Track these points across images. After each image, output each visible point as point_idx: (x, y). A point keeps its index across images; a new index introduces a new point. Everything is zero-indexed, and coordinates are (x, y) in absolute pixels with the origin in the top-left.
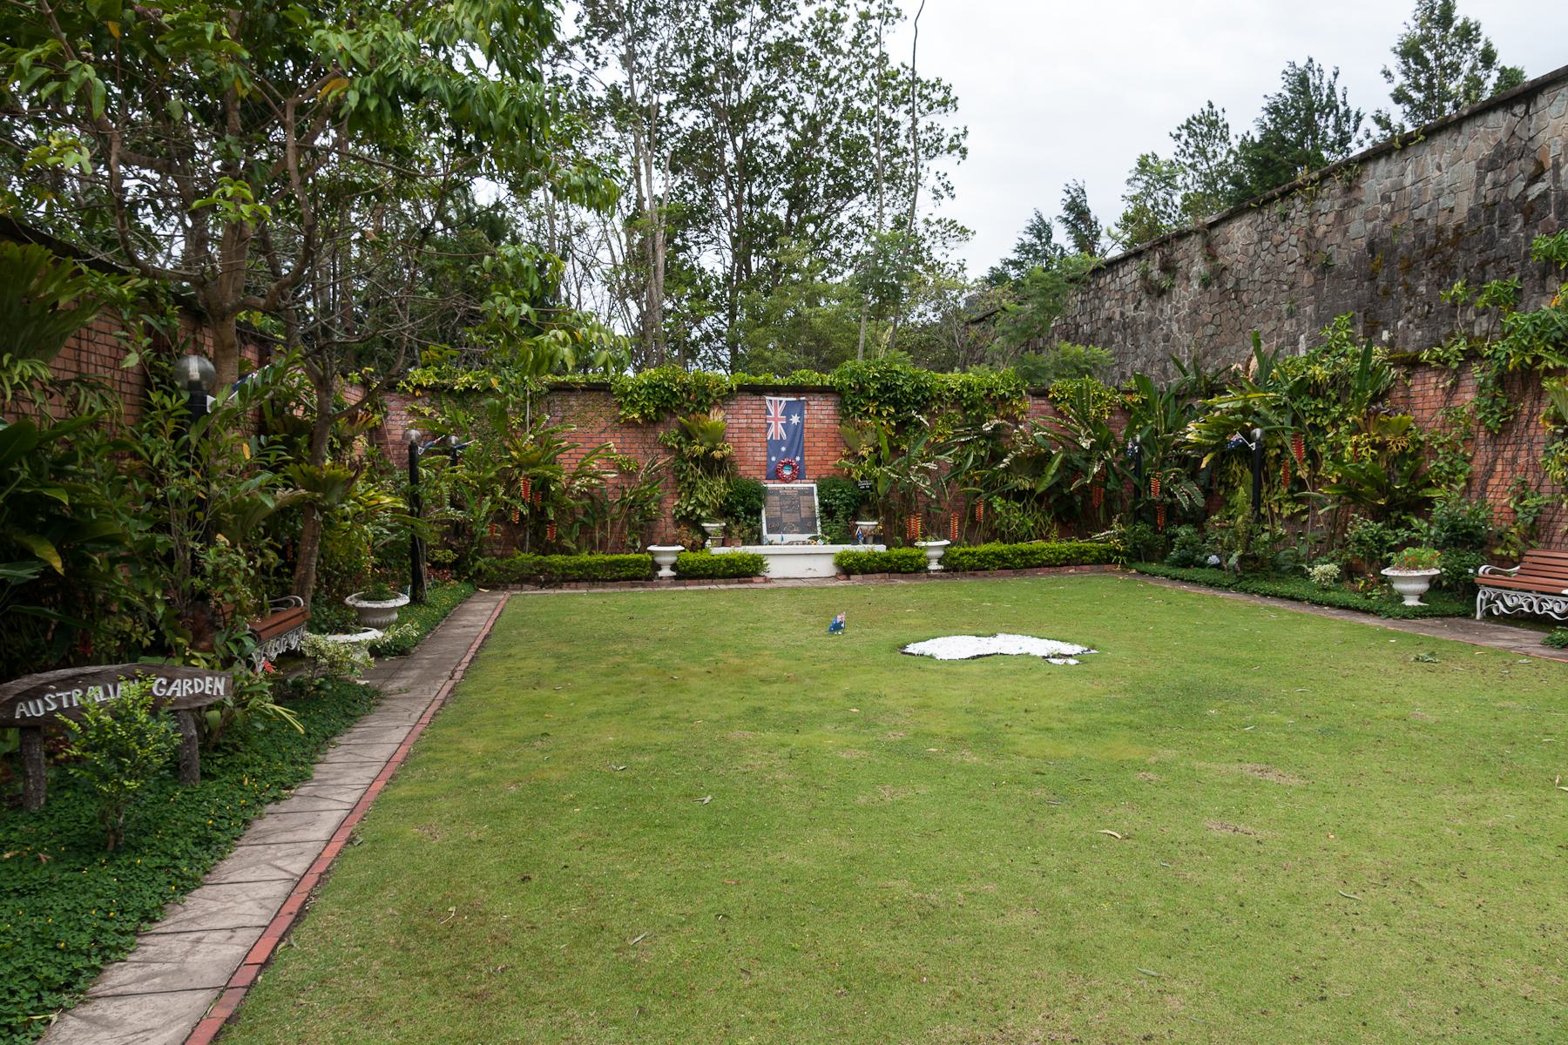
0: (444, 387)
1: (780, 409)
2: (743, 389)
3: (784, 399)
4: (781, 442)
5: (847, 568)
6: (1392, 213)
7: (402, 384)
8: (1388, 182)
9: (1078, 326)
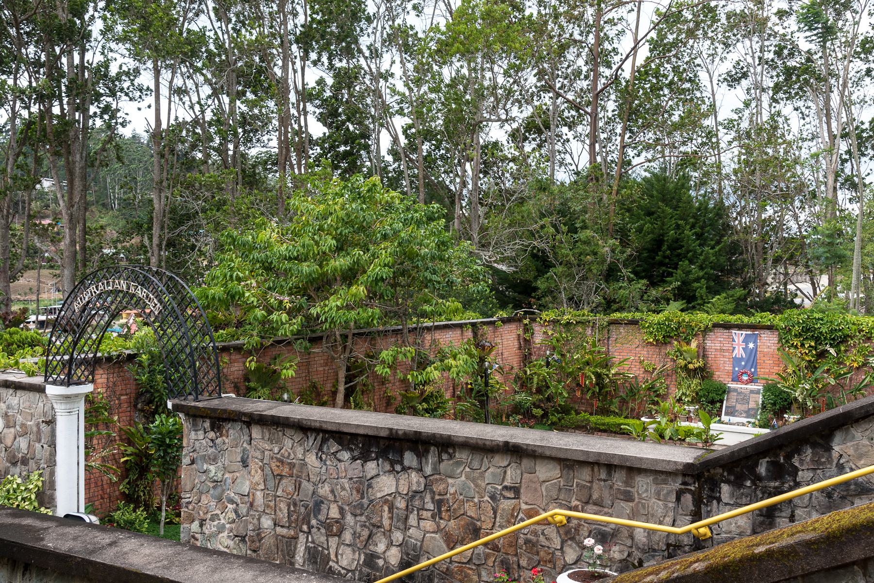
0: (558, 321)
1: (741, 339)
2: (716, 325)
3: (744, 333)
4: (742, 359)
7: (538, 319)
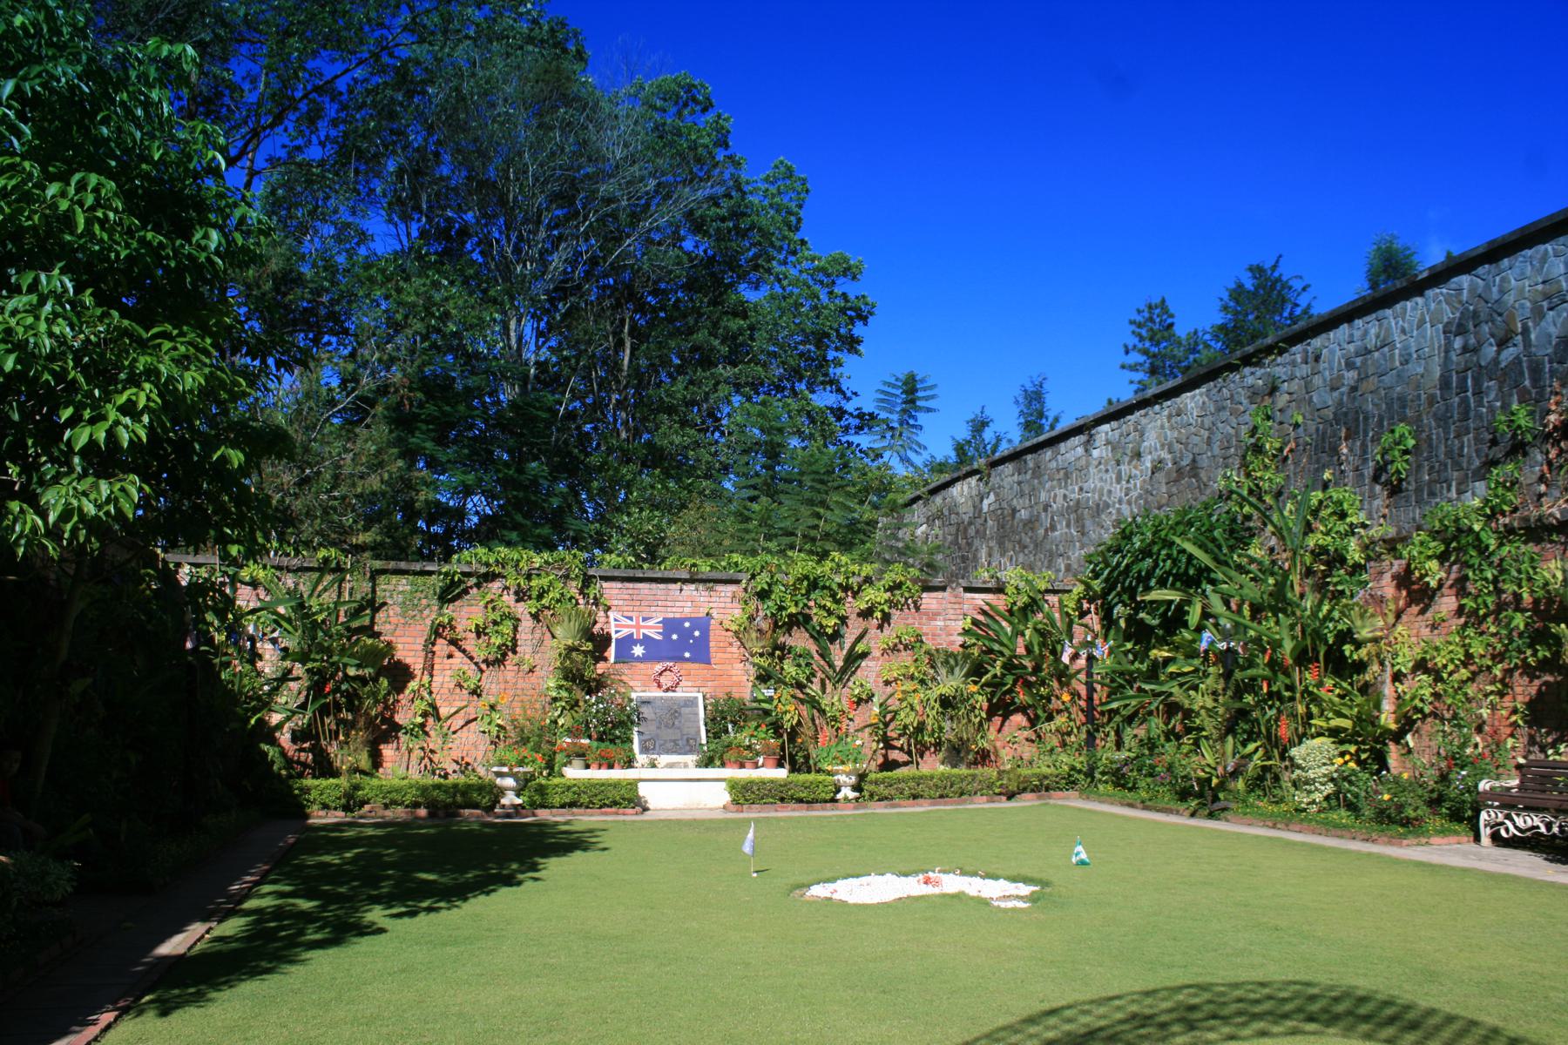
5: (744, 794)
6: (1360, 380)
8: (1351, 347)
9: (1014, 511)
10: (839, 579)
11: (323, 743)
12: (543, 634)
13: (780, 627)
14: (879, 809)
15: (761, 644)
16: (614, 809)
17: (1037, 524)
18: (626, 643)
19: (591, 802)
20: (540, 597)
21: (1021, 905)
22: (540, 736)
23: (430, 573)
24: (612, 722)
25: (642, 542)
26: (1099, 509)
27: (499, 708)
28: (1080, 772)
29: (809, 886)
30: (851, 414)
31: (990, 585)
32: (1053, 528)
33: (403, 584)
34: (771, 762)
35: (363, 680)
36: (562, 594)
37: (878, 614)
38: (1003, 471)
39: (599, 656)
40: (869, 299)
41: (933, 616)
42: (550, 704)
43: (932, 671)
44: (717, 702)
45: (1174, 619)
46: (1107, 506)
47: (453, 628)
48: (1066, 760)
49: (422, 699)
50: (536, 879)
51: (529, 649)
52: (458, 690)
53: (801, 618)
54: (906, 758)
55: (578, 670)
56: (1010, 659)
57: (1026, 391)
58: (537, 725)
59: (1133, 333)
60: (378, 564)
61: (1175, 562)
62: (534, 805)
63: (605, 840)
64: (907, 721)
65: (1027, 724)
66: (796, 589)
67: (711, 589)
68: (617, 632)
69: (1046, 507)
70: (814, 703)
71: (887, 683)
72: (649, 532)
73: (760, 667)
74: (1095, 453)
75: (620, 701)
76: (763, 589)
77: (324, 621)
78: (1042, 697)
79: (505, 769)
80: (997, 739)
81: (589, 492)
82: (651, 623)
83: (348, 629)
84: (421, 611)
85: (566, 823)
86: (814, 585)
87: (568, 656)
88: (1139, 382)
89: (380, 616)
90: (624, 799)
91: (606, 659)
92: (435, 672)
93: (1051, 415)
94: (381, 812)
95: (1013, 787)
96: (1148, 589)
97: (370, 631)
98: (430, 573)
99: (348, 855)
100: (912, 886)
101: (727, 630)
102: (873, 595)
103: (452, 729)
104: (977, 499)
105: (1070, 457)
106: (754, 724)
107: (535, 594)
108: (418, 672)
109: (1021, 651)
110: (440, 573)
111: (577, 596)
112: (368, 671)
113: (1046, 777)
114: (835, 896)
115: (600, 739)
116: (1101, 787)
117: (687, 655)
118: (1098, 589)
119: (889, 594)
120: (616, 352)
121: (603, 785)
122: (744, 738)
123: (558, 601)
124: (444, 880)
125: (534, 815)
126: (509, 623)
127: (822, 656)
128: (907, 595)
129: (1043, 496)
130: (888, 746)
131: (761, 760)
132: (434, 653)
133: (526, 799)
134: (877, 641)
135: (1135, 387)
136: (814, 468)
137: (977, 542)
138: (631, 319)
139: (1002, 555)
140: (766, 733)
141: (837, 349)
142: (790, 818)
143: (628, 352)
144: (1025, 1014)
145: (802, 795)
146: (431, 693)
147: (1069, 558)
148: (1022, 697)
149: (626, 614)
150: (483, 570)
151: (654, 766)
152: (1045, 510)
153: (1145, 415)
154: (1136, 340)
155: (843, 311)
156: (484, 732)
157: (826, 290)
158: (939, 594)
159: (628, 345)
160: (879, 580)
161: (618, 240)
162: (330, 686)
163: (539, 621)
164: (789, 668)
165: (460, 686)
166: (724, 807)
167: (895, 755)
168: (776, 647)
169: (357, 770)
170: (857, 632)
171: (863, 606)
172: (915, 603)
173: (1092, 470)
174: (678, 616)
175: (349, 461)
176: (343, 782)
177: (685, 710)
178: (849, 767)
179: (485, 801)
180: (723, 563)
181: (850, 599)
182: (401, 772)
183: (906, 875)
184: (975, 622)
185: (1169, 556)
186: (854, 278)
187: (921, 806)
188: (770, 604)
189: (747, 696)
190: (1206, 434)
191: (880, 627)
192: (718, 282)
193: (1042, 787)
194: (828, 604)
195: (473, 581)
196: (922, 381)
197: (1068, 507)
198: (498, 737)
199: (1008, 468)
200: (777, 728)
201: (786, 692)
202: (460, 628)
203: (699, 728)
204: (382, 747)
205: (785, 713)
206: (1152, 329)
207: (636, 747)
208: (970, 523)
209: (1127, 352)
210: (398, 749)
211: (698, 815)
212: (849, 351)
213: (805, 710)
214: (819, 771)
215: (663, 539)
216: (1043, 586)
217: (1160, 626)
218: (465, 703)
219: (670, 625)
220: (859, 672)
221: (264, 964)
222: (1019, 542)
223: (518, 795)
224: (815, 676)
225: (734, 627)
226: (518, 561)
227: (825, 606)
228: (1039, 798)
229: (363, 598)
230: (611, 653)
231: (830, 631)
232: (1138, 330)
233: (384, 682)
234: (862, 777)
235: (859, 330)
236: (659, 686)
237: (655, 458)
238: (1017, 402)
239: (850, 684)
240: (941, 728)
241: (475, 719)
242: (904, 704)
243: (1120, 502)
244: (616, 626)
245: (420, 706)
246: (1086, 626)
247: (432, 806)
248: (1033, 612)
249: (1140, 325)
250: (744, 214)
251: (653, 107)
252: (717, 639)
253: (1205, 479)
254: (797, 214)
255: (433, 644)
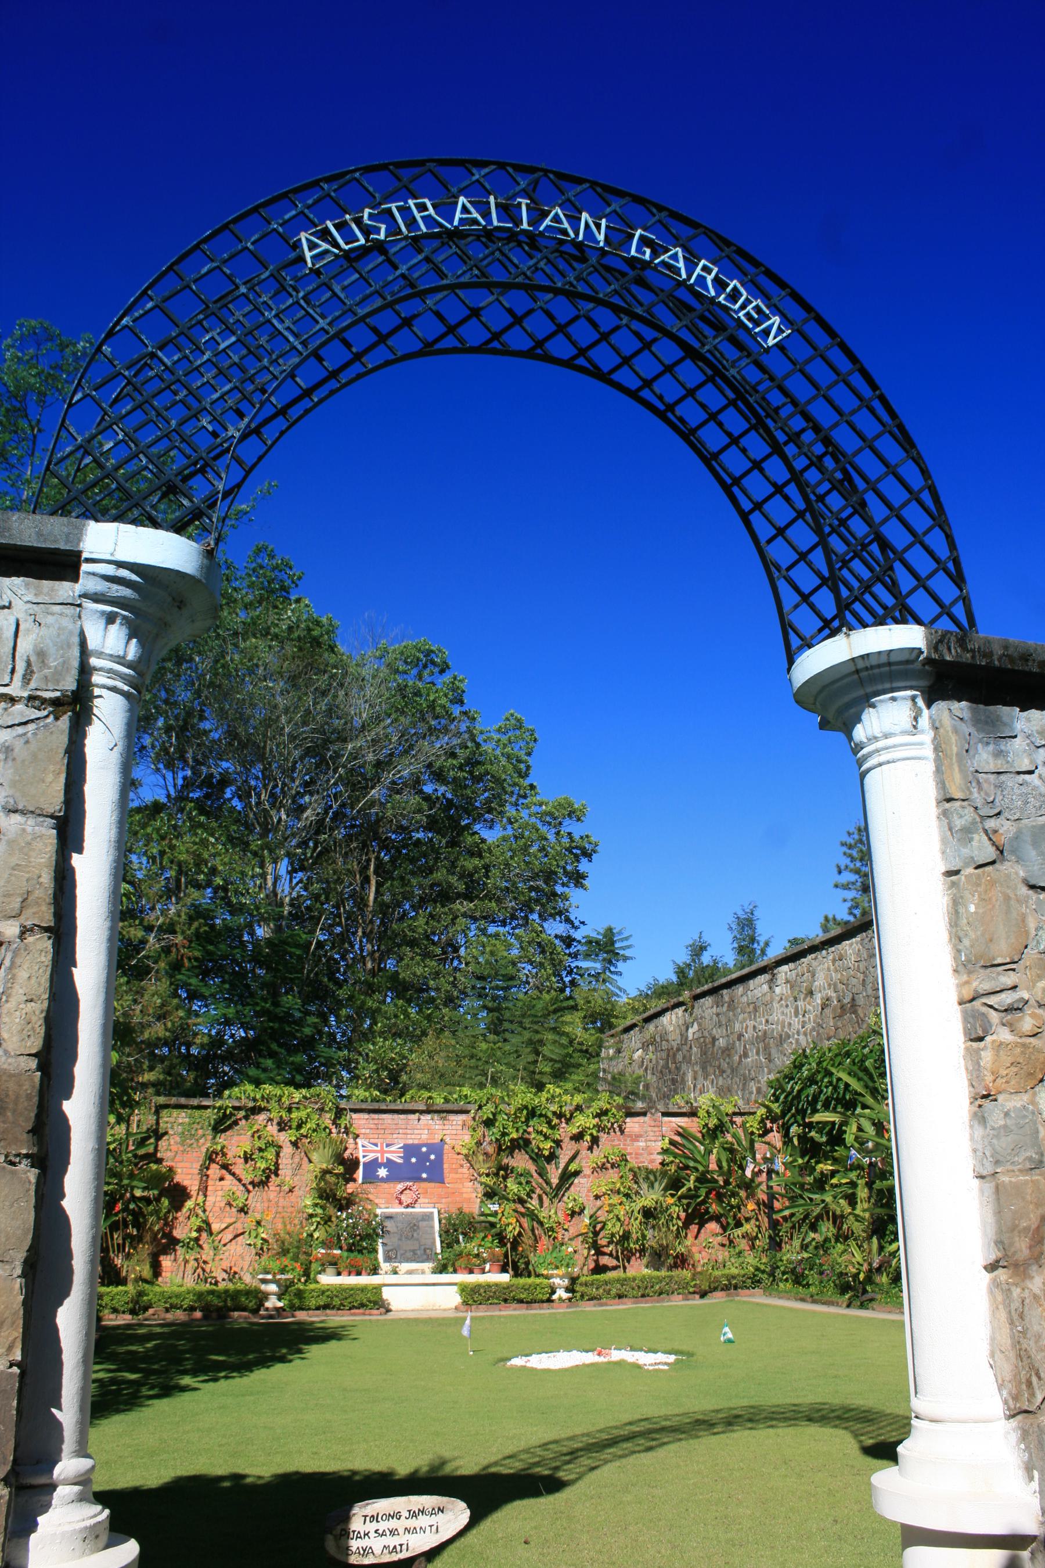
5: (473, 1296)
9: (714, 1040)
10: (554, 1108)
11: (112, 1255)
12: (301, 1159)
13: (504, 1151)
14: (589, 1307)
15: (487, 1166)
16: (361, 1311)
17: (733, 1052)
18: (372, 1166)
19: (342, 1304)
20: (299, 1127)
21: (666, 1367)
22: (298, 1247)
23: (206, 1107)
24: (359, 1235)
25: (386, 1068)
26: (782, 1039)
27: (263, 1224)
28: (763, 1272)
29: (510, 1360)
30: (579, 942)
31: (684, 1110)
32: (745, 1055)
33: (182, 1117)
34: (496, 1268)
35: (147, 1201)
36: (318, 1125)
37: (588, 1138)
38: (704, 1004)
39: (349, 1175)
40: (592, 839)
41: (637, 1138)
42: (307, 1219)
43: (635, 1186)
44: (450, 1217)
45: (836, 1138)
46: (789, 1037)
47: (224, 1155)
48: (751, 1259)
49: (197, 1216)
50: (303, 1359)
51: (289, 1172)
52: (228, 1208)
53: (521, 1142)
54: (614, 1263)
55: (331, 1190)
56: (703, 1174)
57: (738, 918)
58: (296, 1238)
59: (845, 854)
60: (162, 1100)
61: (836, 1088)
62: (293, 1308)
63: (355, 1333)
64: (614, 1230)
65: (721, 1231)
66: (517, 1117)
67: (444, 1119)
68: (364, 1156)
69: (740, 1036)
70: (532, 1216)
71: (597, 1197)
72: (393, 1059)
73: (486, 1185)
74: (778, 990)
75: (367, 1216)
76: (488, 1118)
77: (115, 1149)
78: (732, 1207)
79: (269, 1277)
80: (693, 1245)
81: (337, 1017)
82: (393, 1148)
83: (135, 1156)
84: (197, 1140)
85: (322, 1322)
86: (532, 1113)
87: (322, 1178)
88: (852, 900)
89: (162, 1144)
90: (370, 1302)
91: (355, 1180)
92: (208, 1193)
93: (762, 940)
94: (163, 1315)
95: (705, 1286)
96: (815, 1111)
97: (153, 1157)
98: (206, 1107)
99: (149, 1345)
100: (590, 1358)
101: (459, 1154)
102: (582, 1121)
103: (222, 1242)
104: (683, 1028)
105: (758, 993)
106: (482, 1235)
107: (294, 1124)
108: (194, 1193)
109: (713, 1166)
110: (214, 1108)
111: (331, 1126)
112: (153, 1193)
113: (734, 1277)
114: (528, 1365)
115: (350, 1250)
116: (781, 1285)
117: (424, 1176)
118: (778, 1111)
119: (597, 1120)
120: (363, 888)
121: (352, 1289)
122: (473, 1247)
123: (314, 1131)
124: (231, 1360)
125: (293, 1316)
126: (272, 1150)
127: (540, 1175)
128: (612, 1120)
129: (737, 1027)
130: (599, 1252)
131: (487, 1267)
132: (208, 1176)
133: (286, 1302)
134: (588, 1160)
135: (849, 904)
136: (533, 1012)
137: (684, 1067)
138: (377, 858)
139: (705, 1079)
140: (492, 1242)
141: (563, 885)
142: (511, 1315)
143: (373, 889)
144: (628, 1421)
145: (522, 1296)
146: (204, 1211)
147: (759, 1082)
148: (714, 1208)
149: (372, 1141)
150: (251, 1104)
151: (395, 1273)
152: (739, 1039)
153: (815, 959)
154: (848, 861)
155: (569, 850)
156: (250, 1245)
157: (554, 830)
158: (641, 1119)
159: (373, 882)
160: (589, 1108)
161: (366, 789)
162: (120, 1206)
163: (298, 1148)
164: (512, 1186)
165: (230, 1204)
166: (456, 1308)
167: (605, 1260)
168: (501, 1168)
169: (141, 1279)
170: (570, 1154)
171: (575, 1131)
172: (620, 1127)
173: (775, 1005)
174: (416, 1142)
175: (138, 1012)
176: (130, 1288)
177: (422, 1224)
178: (562, 1271)
179: (252, 1304)
180: (455, 1096)
181: (564, 1125)
182: (178, 1280)
183: (587, 1351)
184: (672, 1143)
185: (830, 1083)
186: (579, 819)
187: (625, 1304)
188: (495, 1130)
189: (476, 1211)
190: (862, 977)
191: (590, 1149)
192: (454, 822)
193: (731, 1286)
194: (545, 1130)
195: (242, 1113)
196: (620, 933)
197: (757, 1037)
198: (262, 1249)
199: (708, 1001)
200: (501, 1238)
201: (509, 1207)
202: (230, 1155)
203: (434, 1239)
204: (162, 1258)
205: (508, 1225)
206: (861, 851)
207: (380, 1256)
208: (678, 1050)
209: (840, 872)
210: (175, 1260)
211: (433, 1315)
212: (576, 886)
213: (526, 1222)
214: (538, 1276)
215: (405, 1065)
216: (730, 1109)
217: (827, 1143)
218: (233, 1220)
219: (410, 1150)
220: (572, 1188)
221: (122, 1407)
222: (719, 1067)
223: (279, 1300)
224: (534, 1192)
225: (465, 1151)
226: (281, 1097)
227: (541, 1132)
228: (728, 1295)
229: (148, 1129)
230: (360, 1174)
231: (546, 1153)
232: (848, 851)
233: (165, 1202)
234: (574, 1280)
235: (584, 866)
236: (401, 1203)
237: (402, 988)
238: (731, 929)
239: (565, 1199)
240: (644, 1236)
241: (243, 1233)
242: (611, 1215)
243: (798, 1033)
244: (364, 1151)
245: (195, 1222)
246: (768, 1143)
247: (207, 1309)
248: (722, 1132)
249: (850, 847)
250: (479, 763)
251: (397, 671)
252: (450, 1161)
253: (862, 1015)
254: (526, 762)
255: (208, 1168)
